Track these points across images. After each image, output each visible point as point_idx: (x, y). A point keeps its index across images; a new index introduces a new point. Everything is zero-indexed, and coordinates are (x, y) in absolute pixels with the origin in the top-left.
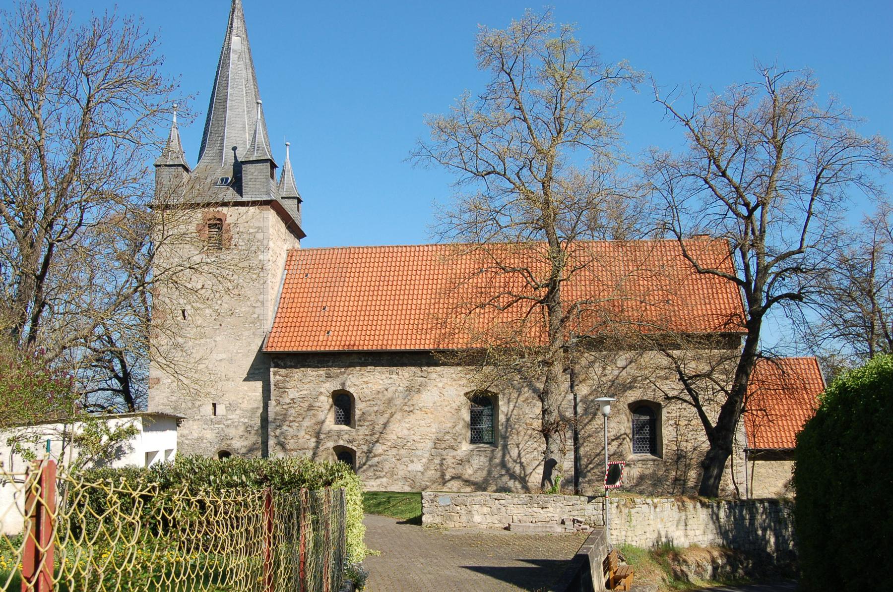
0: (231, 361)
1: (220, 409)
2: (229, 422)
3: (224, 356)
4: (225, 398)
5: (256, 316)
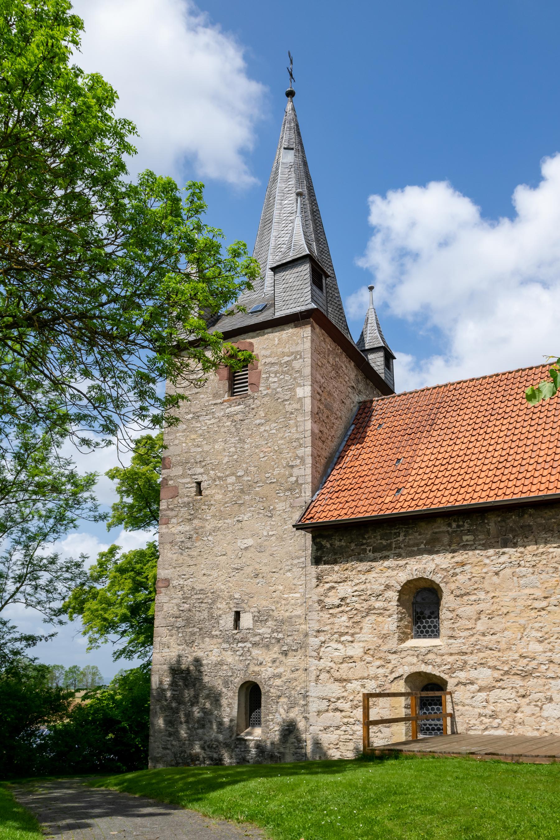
0: (260, 549)
1: (246, 621)
2: (257, 639)
3: (250, 542)
4: (254, 602)
5: (294, 479)
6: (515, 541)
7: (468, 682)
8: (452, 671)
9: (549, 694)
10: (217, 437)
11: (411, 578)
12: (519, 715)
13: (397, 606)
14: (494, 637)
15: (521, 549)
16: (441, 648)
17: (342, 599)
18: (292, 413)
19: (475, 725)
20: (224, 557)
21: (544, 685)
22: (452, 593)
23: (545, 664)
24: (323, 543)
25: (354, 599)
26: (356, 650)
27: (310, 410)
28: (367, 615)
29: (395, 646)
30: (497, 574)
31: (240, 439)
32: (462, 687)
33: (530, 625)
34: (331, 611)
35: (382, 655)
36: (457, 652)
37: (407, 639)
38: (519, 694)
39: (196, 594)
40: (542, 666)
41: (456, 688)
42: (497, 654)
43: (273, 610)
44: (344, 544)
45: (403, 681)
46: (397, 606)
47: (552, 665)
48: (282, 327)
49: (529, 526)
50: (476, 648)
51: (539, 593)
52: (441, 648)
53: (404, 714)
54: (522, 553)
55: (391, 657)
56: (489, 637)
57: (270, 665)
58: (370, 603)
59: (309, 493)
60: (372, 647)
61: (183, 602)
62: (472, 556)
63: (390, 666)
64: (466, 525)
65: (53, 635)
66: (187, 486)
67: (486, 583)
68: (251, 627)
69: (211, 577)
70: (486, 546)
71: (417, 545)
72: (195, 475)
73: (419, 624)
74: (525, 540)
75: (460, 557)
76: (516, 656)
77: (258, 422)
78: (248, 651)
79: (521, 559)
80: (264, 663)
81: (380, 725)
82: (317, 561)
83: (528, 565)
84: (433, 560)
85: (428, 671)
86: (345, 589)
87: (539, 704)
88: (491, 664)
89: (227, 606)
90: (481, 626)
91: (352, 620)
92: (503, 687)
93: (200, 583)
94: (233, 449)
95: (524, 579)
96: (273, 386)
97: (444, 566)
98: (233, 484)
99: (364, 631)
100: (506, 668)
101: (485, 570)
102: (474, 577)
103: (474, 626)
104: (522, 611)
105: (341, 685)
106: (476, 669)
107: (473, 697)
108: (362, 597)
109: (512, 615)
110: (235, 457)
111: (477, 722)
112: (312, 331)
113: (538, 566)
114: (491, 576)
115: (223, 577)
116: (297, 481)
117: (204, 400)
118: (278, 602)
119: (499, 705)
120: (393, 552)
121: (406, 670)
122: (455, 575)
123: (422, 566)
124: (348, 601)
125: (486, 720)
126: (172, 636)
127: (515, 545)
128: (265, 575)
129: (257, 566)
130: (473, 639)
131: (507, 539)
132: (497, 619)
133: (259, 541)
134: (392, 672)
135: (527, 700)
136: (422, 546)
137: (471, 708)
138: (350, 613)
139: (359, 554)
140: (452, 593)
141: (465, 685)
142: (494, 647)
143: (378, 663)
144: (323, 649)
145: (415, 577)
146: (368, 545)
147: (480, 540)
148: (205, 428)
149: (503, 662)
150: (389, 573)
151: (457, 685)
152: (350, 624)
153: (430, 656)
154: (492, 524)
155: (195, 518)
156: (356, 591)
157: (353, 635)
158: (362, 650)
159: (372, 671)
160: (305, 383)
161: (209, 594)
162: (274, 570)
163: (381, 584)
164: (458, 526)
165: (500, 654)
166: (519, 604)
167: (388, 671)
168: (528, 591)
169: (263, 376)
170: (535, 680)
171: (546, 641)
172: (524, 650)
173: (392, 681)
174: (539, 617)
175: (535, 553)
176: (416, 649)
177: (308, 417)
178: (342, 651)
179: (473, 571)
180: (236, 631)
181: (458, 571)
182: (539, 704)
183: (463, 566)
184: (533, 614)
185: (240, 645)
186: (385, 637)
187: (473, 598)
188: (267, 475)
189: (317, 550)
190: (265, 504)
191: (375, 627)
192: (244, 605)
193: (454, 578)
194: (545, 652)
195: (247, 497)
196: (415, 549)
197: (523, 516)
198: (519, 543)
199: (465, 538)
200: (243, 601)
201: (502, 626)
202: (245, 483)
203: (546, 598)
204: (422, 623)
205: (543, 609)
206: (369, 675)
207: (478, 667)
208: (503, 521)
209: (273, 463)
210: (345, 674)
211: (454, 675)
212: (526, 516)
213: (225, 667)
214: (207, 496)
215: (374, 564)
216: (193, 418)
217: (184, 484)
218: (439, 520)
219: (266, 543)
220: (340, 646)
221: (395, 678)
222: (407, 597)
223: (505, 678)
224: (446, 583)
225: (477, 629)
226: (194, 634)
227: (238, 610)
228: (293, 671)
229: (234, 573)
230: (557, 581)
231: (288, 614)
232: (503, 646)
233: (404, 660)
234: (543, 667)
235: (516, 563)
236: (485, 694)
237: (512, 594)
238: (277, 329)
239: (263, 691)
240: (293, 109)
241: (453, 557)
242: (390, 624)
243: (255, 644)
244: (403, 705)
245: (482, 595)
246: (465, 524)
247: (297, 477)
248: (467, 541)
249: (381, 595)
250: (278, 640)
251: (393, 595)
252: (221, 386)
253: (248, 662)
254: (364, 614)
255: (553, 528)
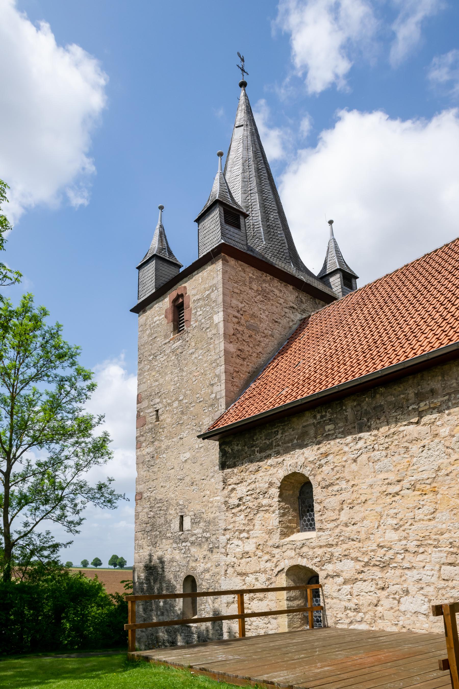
3: (188, 455)
5: (214, 395)
6: (369, 424)
7: (335, 574)
8: (322, 564)
9: (405, 586)
10: (166, 371)
11: (286, 474)
12: (379, 608)
13: (279, 501)
14: (355, 527)
15: (375, 432)
16: (312, 540)
17: (240, 499)
18: (211, 339)
19: (342, 618)
20: (173, 470)
21: (401, 577)
22: (319, 485)
23: (400, 554)
24: (226, 449)
25: (248, 498)
26: (250, 546)
27: (223, 332)
28: (258, 513)
29: (278, 540)
30: (355, 461)
31: (180, 369)
32: (331, 579)
33: (386, 512)
34: (233, 511)
35: (269, 549)
36: (325, 544)
37: (293, 533)
38: (378, 587)
39: (157, 503)
40: (398, 556)
41: (326, 581)
42: (358, 545)
43: (203, 513)
44: (240, 448)
45: (284, 574)
46: (279, 501)
47: (407, 554)
48: (203, 267)
49: (381, 406)
50: (342, 540)
51: (392, 477)
52: (312, 540)
53: (286, 606)
54: (375, 436)
55: (276, 551)
56: (351, 527)
57: (202, 561)
58: (259, 501)
59: (224, 406)
60: (261, 543)
61: (150, 511)
62: (332, 445)
63: (275, 560)
64: (328, 415)
65: (70, 543)
66: (151, 415)
67: (346, 472)
68: (190, 529)
69: (166, 488)
70: (345, 434)
71: (292, 440)
72: (155, 404)
73: (305, 518)
74: (378, 421)
75: (324, 448)
76: (374, 547)
77: (190, 351)
78: (189, 549)
79: (375, 442)
80: (199, 560)
81: (270, 616)
82: (223, 466)
83: (381, 448)
84: (303, 454)
85: (303, 565)
86: (242, 490)
87: (397, 596)
88: (353, 555)
89: (175, 512)
90: (344, 517)
91: (248, 518)
92: (365, 578)
93: (160, 494)
94: (176, 379)
95: (379, 463)
96: (200, 318)
97: (311, 459)
98: (177, 408)
99: (256, 527)
100: (366, 560)
101: (344, 459)
102: (336, 466)
103: (337, 517)
104: (377, 498)
105: (242, 578)
106: (341, 561)
107: (339, 590)
108: (253, 496)
109: (369, 502)
110: (178, 385)
111: (343, 616)
112: (223, 264)
113: (390, 447)
114: (350, 464)
115: (173, 487)
116: (216, 396)
117: (159, 342)
118: (206, 506)
119: (362, 598)
120: (274, 450)
121: (286, 564)
122: (321, 466)
123: (294, 461)
124: (244, 501)
125: (351, 614)
126: (144, 539)
127: (369, 429)
128: (197, 482)
129: (193, 476)
130: (337, 531)
131: (362, 423)
132: (357, 508)
133: (194, 453)
134: (276, 566)
135: (385, 593)
136: (295, 441)
137: (338, 601)
138: (245, 512)
139: (250, 455)
140: (319, 485)
141: (333, 577)
142: (355, 537)
143: (267, 557)
144: (228, 546)
145: (290, 472)
146: (256, 446)
147: (340, 428)
148: (160, 365)
149: (363, 553)
150: (272, 470)
151: (326, 578)
152: (246, 522)
153: (305, 549)
154: (349, 410)
155: (156, 440)
156: (249, 491)
157: (248, 532)
158: (254, 545)
159: (263, 565)
160: (219, 310)
161: (165, 503)
162: (203, 478)
163: (266, 482)
164: (322, 417)
165: (360, 545)
166: (375, 490)
167: (273, 565)
168: (383, 476)
169: (193, 312)
170: (393, 571)
171: (402, 529)
172: (381, 540)
173: (277, 575)
174: (394, 503)
175: (387, 434)
176: (293, 543)
177: (222, 339)
178: (241, 547)
179: (335, 460)
180: (181, 533)
181: (323, 462)
182: (397, 596)
183: (327, 456)
184: (388, 500)
185: (184, 544)
186: (270, 532)
187: (336, 488)
188: (198, 395)
189: (223, 456)
190: (196, 421)
191: (264, 523)
192: (185, 510)
193: (321, 470)
194: (400, 540)
195: (185, 417)
196: (290, 445)
197: (375, 396)
198: (373, 426)
199: (327, 427)
200: (185, 506)
201: (361, 515)
202: (184, 405)
203: (399, 481)
204: (307, 517)
205: (397, 494)
206: (260, 569)
207: (343, 559)
208: (359, 405)
209: (201, 385)
210: (244, 568)
211: (323, 568)
212: (378, 396)
213: (175, 564)
214: (162, 421)
215: (261, 464)
216: (153, 358)
217: (149, 413)
218: (308, 414)
219: (197, 455)
220: (240, 543)
221: (279, 572)
222: (291, 492)
223: (365, 569)
224: (315, 475)
225: (341, 520)
226: (156, 537)
227: (182, 514)
228: (216, 566)
229: (179, 483)
230: (408, 461)
231: (213, 515)
232: (362, 536)
233: (285, 554)
234: (400, 557)
235: (371, 447)
236: (349, 586)
237: (369, 481)
238: (200, 270)
239: (198, 584)
240: (246, 95)
241: (318, 449)
242: (273, 519)
243: (193, 543)
244: (285, 598)
245: (343, 485)
246: (328, 414)
247: (216, 393)
248: (329, 430)
249: (266, 492)
250: (207, 539)
251: (275, 491)
252: (168, 327)
253: (188, 559)
254: (255, 512)
255: (402, 404)
